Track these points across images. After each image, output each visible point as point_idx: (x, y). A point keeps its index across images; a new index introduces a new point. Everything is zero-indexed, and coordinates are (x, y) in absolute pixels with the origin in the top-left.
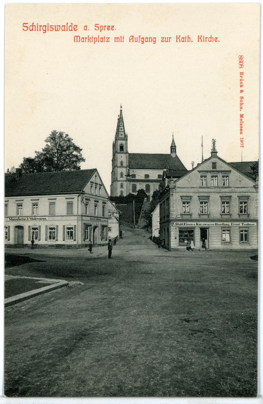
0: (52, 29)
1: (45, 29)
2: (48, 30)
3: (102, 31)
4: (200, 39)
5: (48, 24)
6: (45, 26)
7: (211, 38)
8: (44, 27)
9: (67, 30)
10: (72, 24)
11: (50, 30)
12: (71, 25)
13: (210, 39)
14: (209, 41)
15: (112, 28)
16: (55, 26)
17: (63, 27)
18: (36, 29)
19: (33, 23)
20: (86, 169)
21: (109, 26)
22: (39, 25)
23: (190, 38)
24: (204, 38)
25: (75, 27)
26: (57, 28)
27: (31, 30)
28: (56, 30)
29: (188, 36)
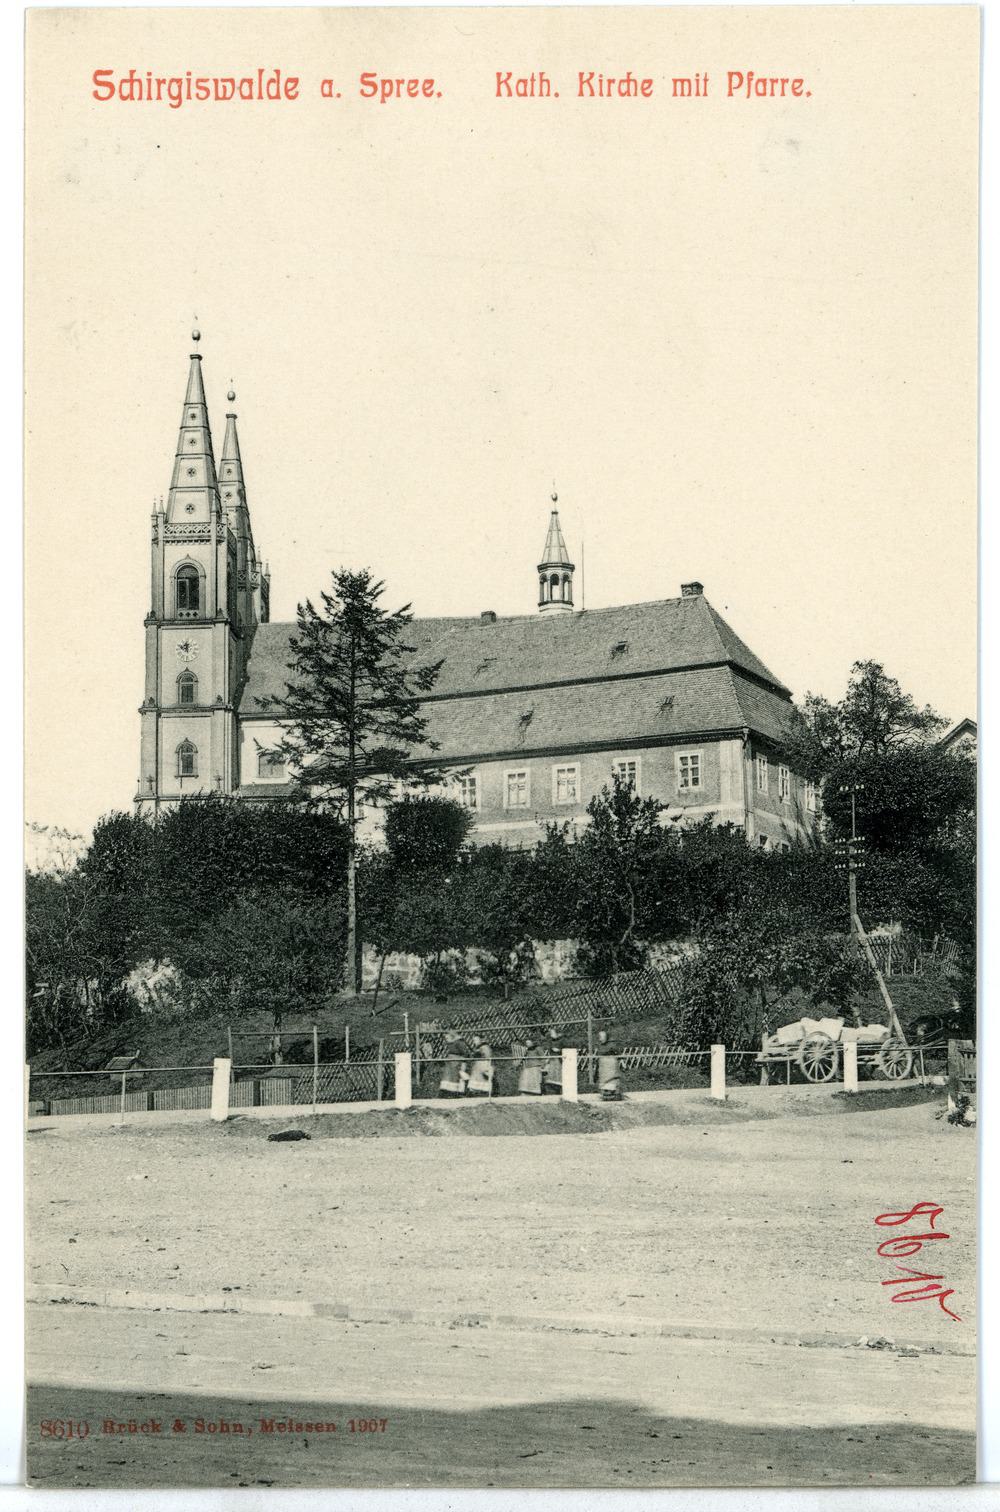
0: (203, 94)
1: (177, 90)
2: (189, 97)
3: (386, 99)
4: (586, 87)
5: (189, 74)
6: (179, 81)
7: (628, 81)
8: (175, 86)
9: (260, 97)
10: (278, 72)
11: (197, 95)
12: (275, 76)
13: (624, 88)
14: (622, 95)
15: (424, 90)
16: (216, 81)
17: (246, 86)
18: (145, 95)
19: (132, 72)
20: (447, 615)
21: (416, 82)
22: (153, 78)
23: (548, 81)
24: (601, 81)
25: (290, 85)
26: (225, 87)
27: (124, 98)
28: (217, 98)
29: (542, 74)
